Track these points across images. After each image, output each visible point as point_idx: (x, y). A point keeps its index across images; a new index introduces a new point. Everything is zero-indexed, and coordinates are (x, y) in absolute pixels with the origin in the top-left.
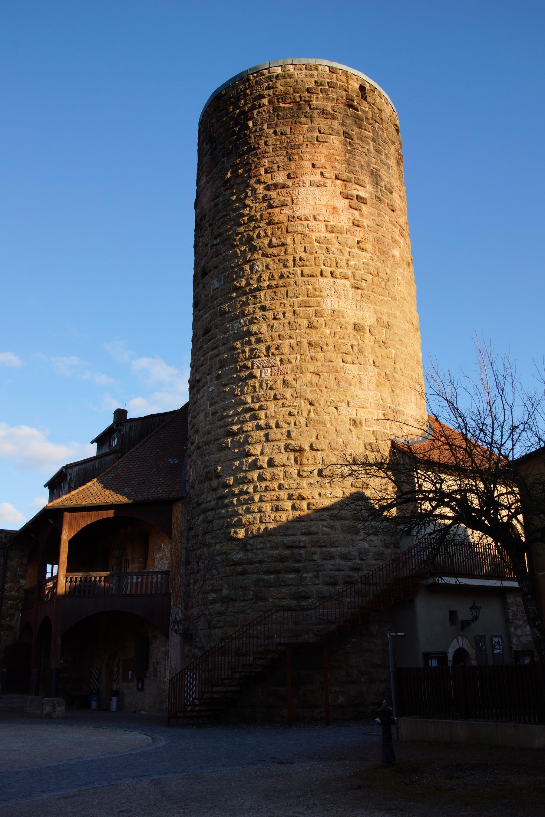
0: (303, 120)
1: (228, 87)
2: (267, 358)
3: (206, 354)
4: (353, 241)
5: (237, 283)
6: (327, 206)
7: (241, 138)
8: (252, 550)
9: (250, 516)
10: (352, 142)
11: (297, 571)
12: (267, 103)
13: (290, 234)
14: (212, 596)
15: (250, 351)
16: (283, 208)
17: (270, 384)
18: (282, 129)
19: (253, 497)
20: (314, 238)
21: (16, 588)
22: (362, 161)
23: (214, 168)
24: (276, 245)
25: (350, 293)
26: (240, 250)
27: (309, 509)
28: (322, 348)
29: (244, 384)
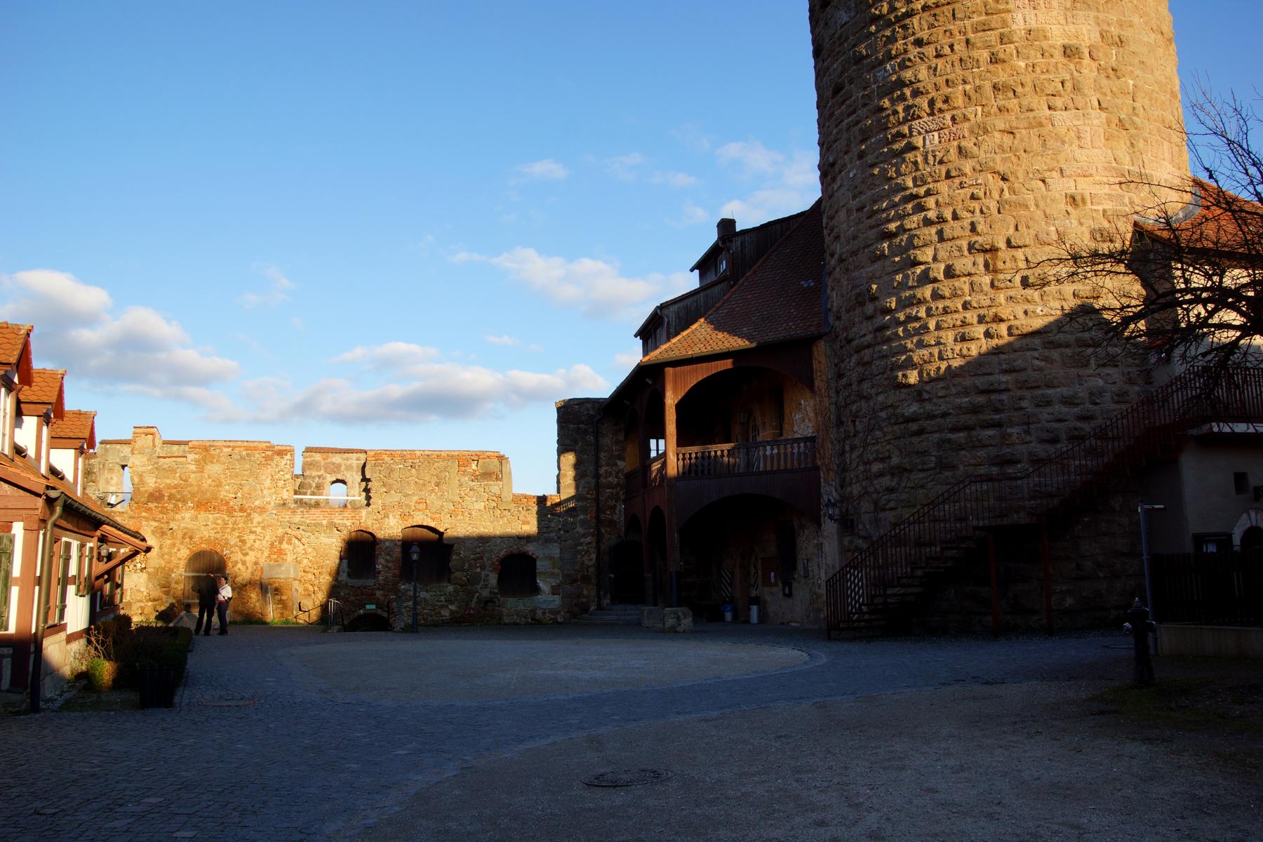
8: (930, 400)
11: (998, 425)
14: (876, 467)
15: (904, 110)
17: (939, 155)
27: (1010, 334)
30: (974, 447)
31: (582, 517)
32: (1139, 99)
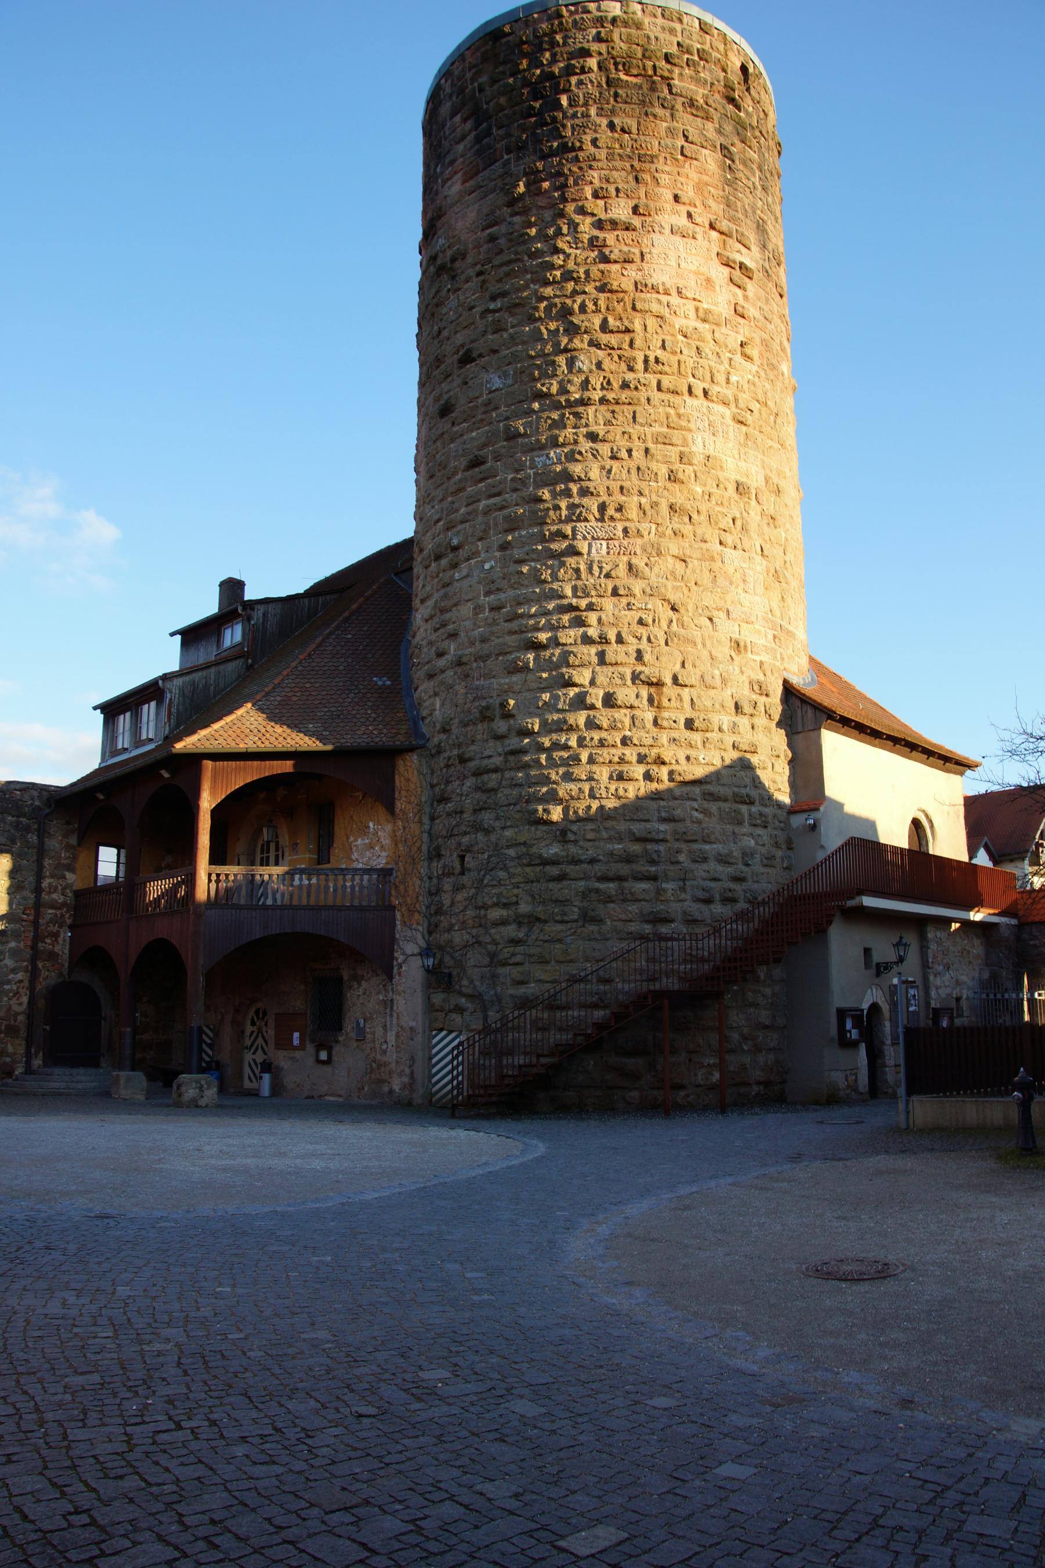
0: (659, 111)
1: (516, 21)
2: (600, 524)
3: (474, 502)
4: (736, 341)
5: (543, 385)
6: (697, 273)
7: (546, 124)
8: (575, 842)
9: (573, 787)
10: (733, 166)
11: (654, 878)
12: (595, 68)
13: (639, 315)
14: (495, 914)
15: (568, 507)
16: (627, 265)
17: (607, 568)
18: (625, 121)
19: (579, 754)
20: (677, 327)
22: (746, 201)
23: (484, 169)
24: (615, 329)
25: (731, 429)
26: (546, 329)
27: (671, 780)
28: (690, 518)
29: (556, 563)
30: (625, 900)
31: (13, 944)
32: (788, 553)
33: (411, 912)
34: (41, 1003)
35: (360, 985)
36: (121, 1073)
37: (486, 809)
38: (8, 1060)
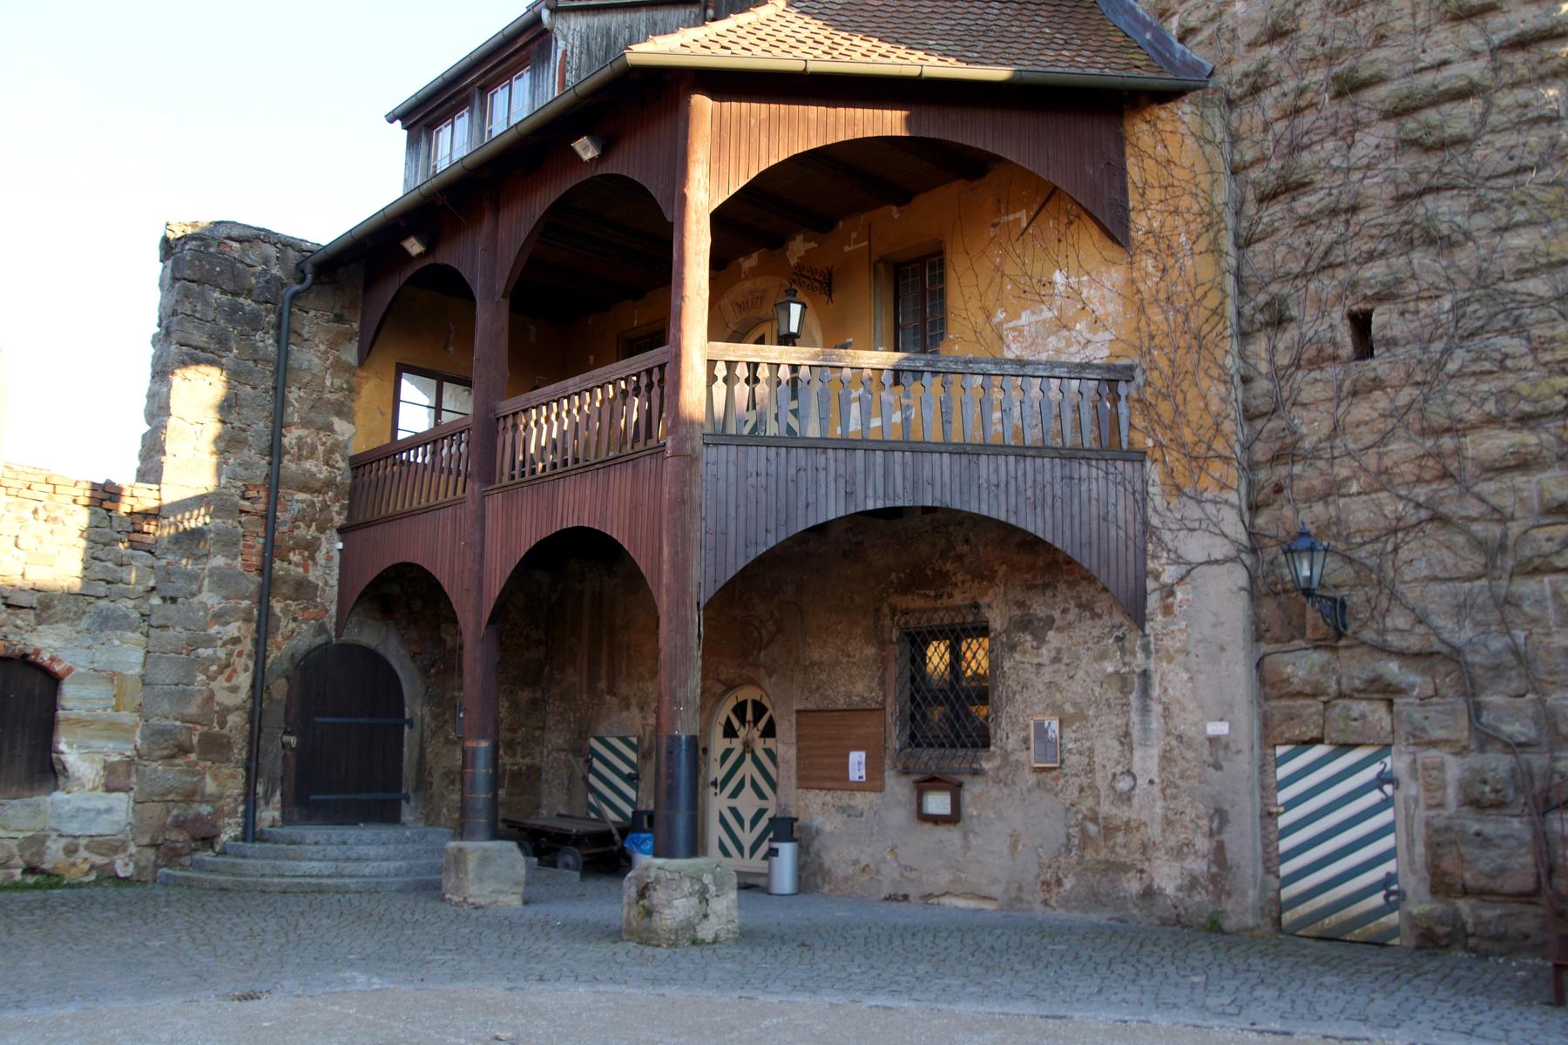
21: (321, 449)
31: (219, 561)
33: (1198, 462)
34: (279, 688)
35: (1041, 640)
36: (467, 845)
37: (1438, 189)
38: (205, 809)
